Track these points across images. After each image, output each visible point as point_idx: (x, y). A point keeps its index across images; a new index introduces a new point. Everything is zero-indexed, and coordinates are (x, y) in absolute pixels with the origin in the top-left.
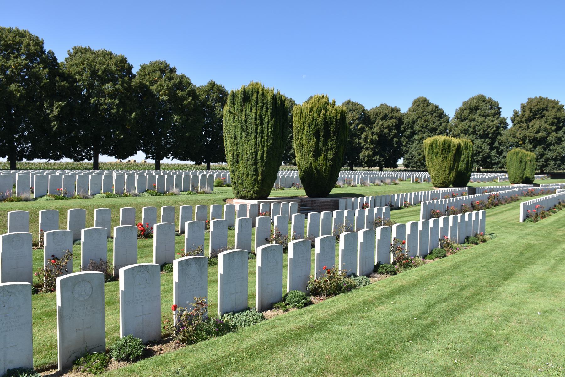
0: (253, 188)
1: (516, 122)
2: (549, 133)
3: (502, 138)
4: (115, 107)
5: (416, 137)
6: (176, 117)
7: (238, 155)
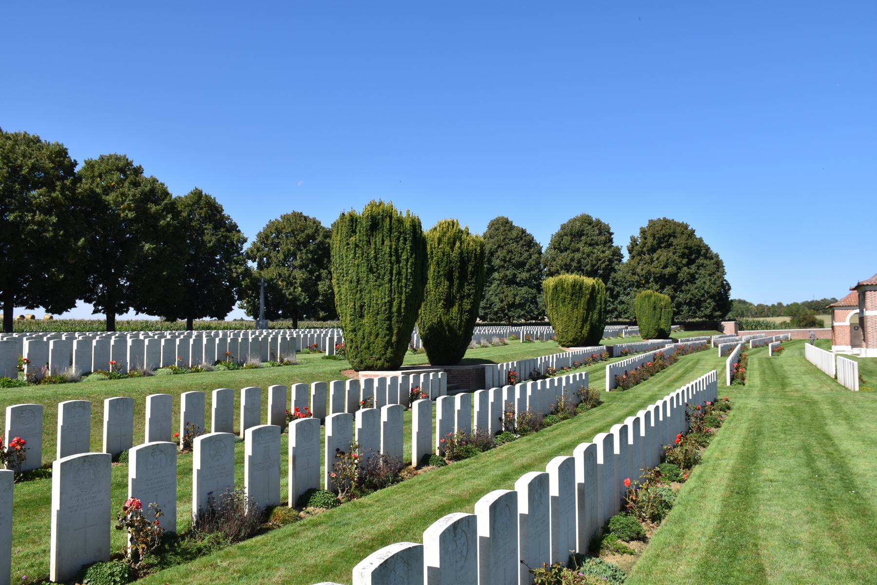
0: (385, 354)
1: (634, 253)
2: (679, 268)
3: (618, 275)
4: (50, 228)
5: (496, 275)
6: (147, 246)
7: (362, 307)
